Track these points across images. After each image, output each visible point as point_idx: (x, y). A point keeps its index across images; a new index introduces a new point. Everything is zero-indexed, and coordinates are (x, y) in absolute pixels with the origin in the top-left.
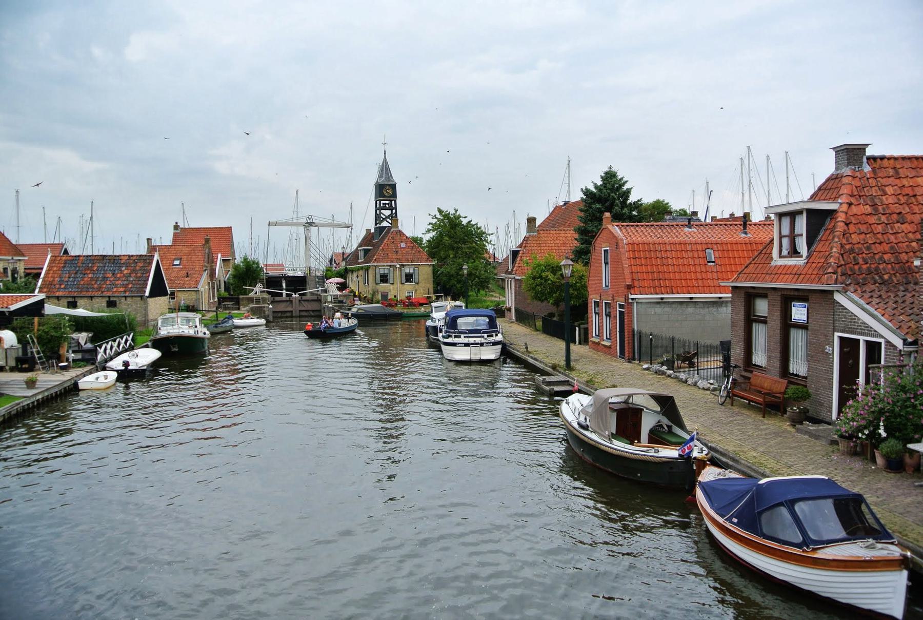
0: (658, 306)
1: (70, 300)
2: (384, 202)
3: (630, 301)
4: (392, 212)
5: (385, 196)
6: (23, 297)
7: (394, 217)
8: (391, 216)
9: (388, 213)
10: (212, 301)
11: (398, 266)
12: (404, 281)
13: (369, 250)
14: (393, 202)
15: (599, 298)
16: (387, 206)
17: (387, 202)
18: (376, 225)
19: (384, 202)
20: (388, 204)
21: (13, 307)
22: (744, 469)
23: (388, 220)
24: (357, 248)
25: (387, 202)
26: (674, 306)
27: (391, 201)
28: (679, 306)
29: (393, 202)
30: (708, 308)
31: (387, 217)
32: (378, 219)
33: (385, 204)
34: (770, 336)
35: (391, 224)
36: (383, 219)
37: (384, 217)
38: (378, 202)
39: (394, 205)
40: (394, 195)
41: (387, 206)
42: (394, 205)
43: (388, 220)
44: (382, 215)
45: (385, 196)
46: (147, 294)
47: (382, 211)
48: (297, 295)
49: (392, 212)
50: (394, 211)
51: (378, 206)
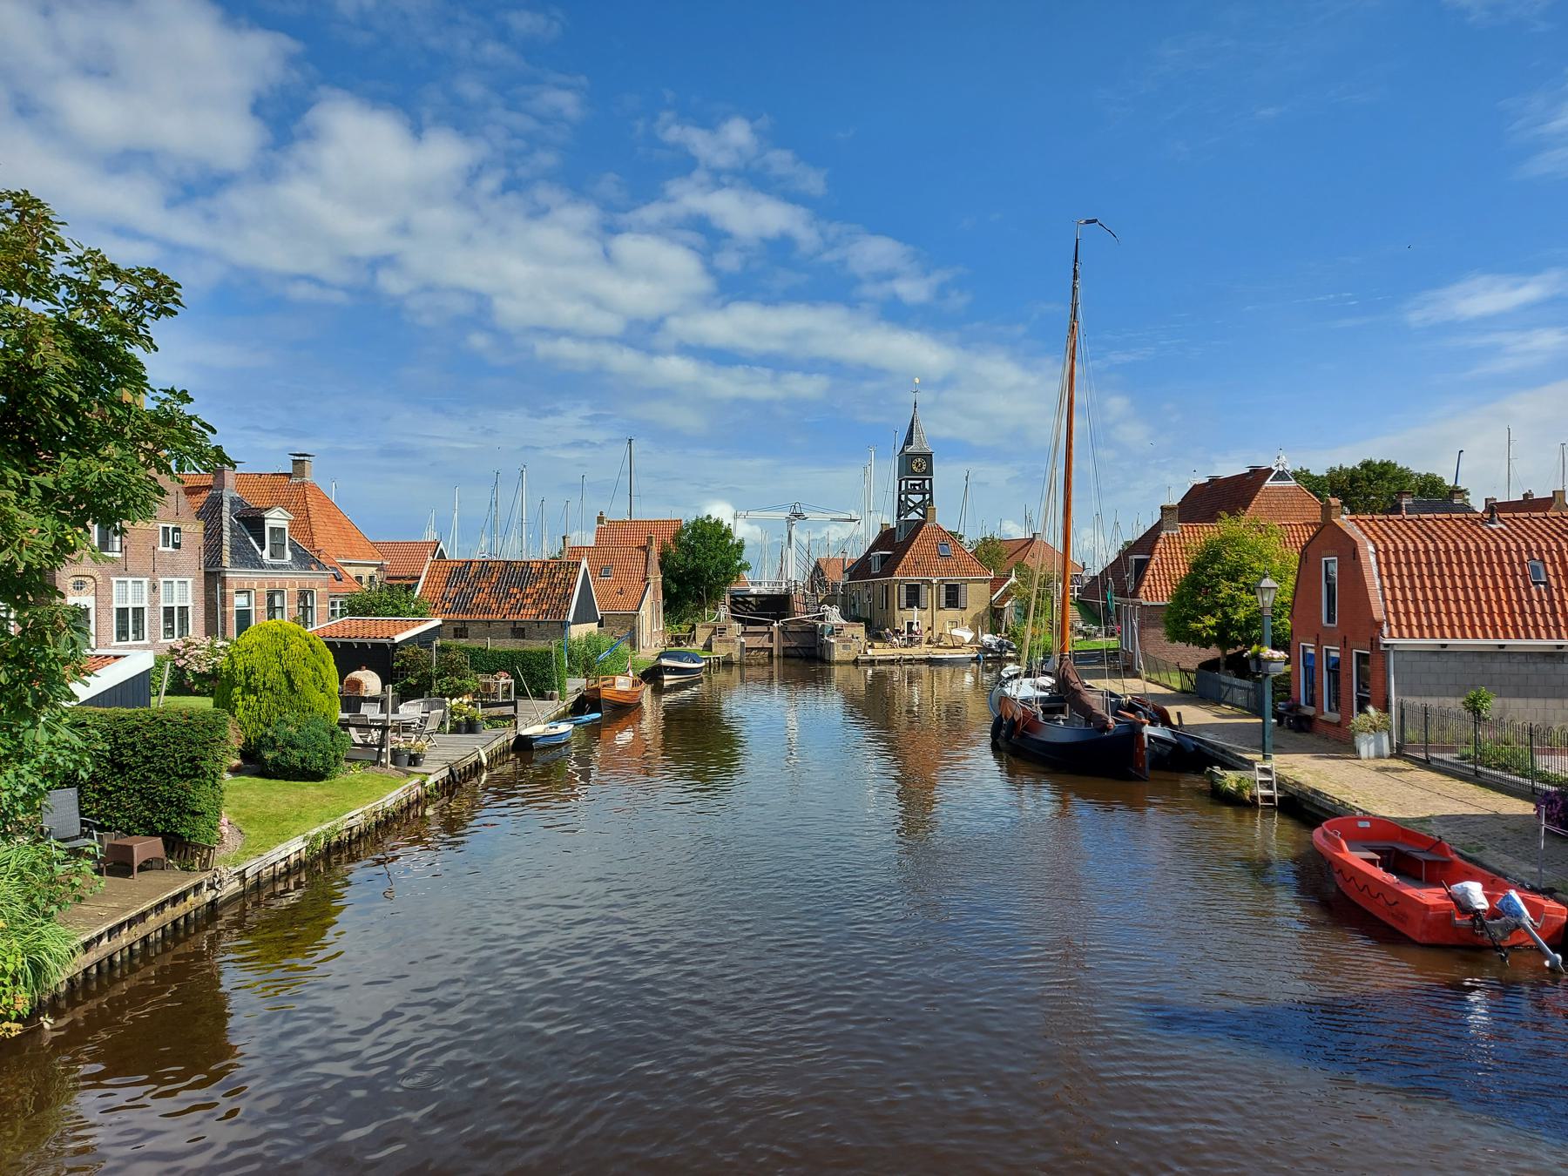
0: (1435, 658)
1: (458, 625)
2: (913, 482)
3: (1382, 648)
4: (924, 497)
5: (914, 473)
6: (416, 623)
7: (927, 505)
8: (922, 504)
9: (917, 498)
10: (655, 630)
11: (935, 581)
12: (943, 604)
14: (927, 482)
15: (1315, 641)
16: (917, 488)
17: (917, 482)
18: (899, 516)
19: (913, 482)
20: (919, 485)
21: (398, 639)
22: (1121, 1064)
23: (919, 510)
24: (868, 554)
25: (917, 482)
26: (1466, 659)
27: (924, 480)
28: (1477, 659)
29: (927, 482)
30: (1535, 663)
31: (916, 505)
32: (903, 508)
33: (915, 485)
34: (549, 666)
35: (923, 516)
36: (911, 508)
37: (912, 505)
38: (903, 482)
39: (927, 487)
40: (929, 471)
41: (917, 488)
42: (927, 487)
43: (919, 510)
44: (909, 503)
45: (914, 473)
46: (570, 619)
47: (909, 496)
48: (780, 624)
49: (924, 497)
50: (927, 496)
51: (903, 488)
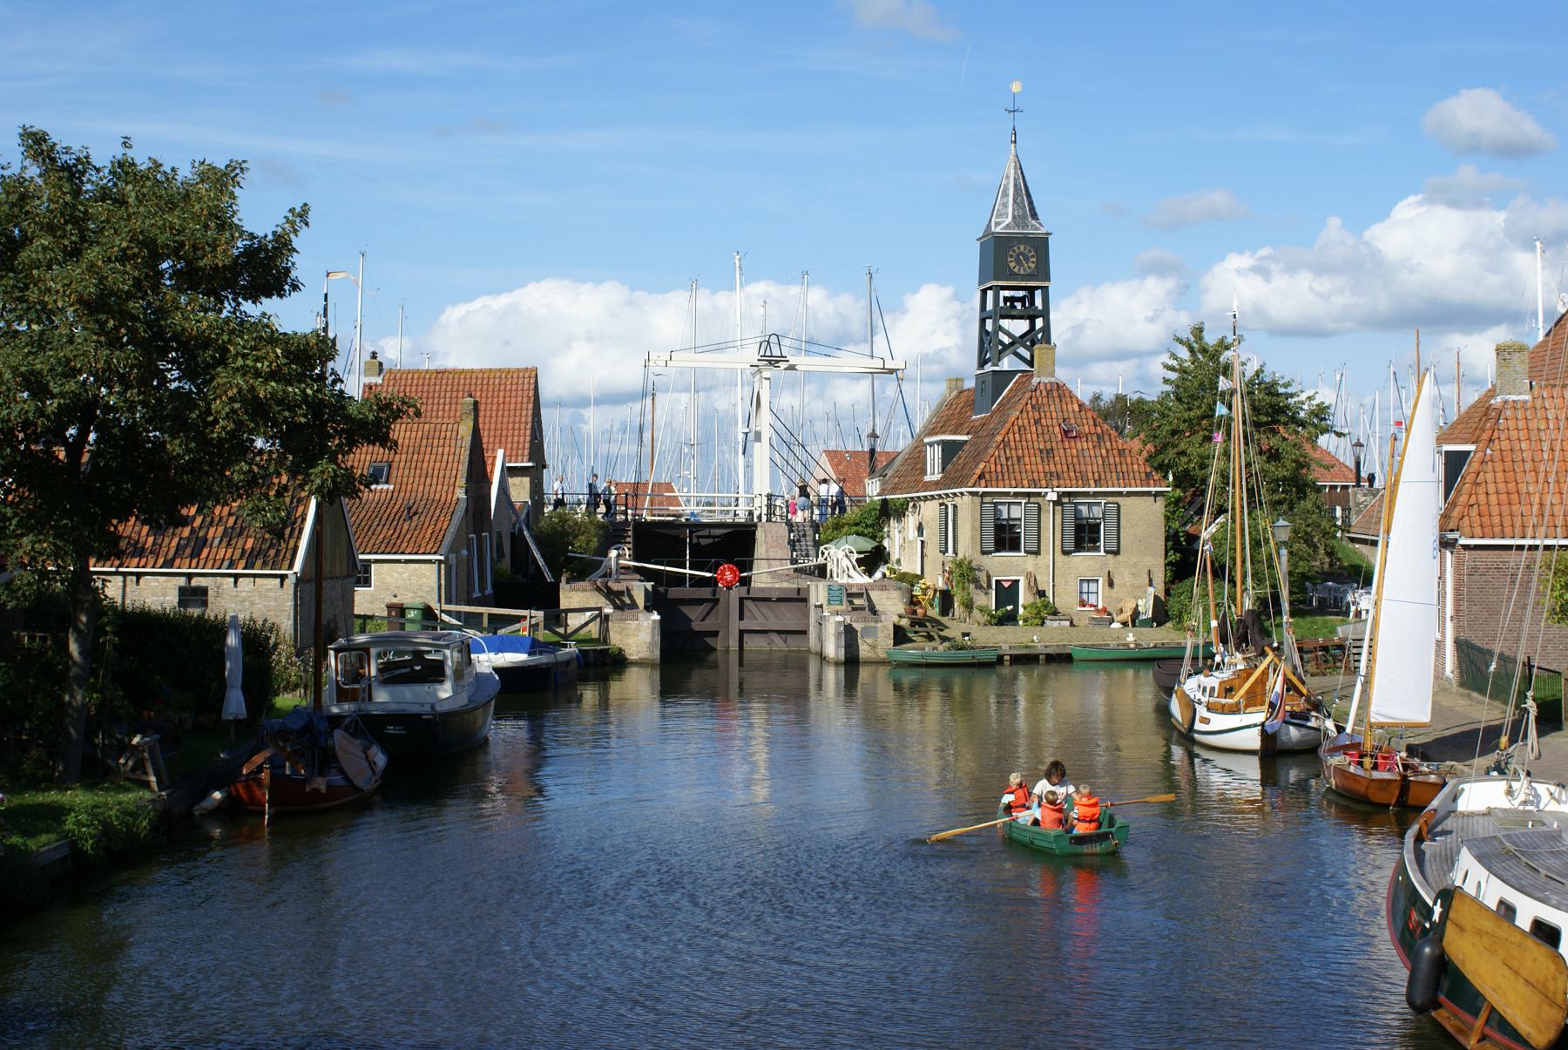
13: (959, 445)
20: (1022, 300)
40: (1043, 272)
